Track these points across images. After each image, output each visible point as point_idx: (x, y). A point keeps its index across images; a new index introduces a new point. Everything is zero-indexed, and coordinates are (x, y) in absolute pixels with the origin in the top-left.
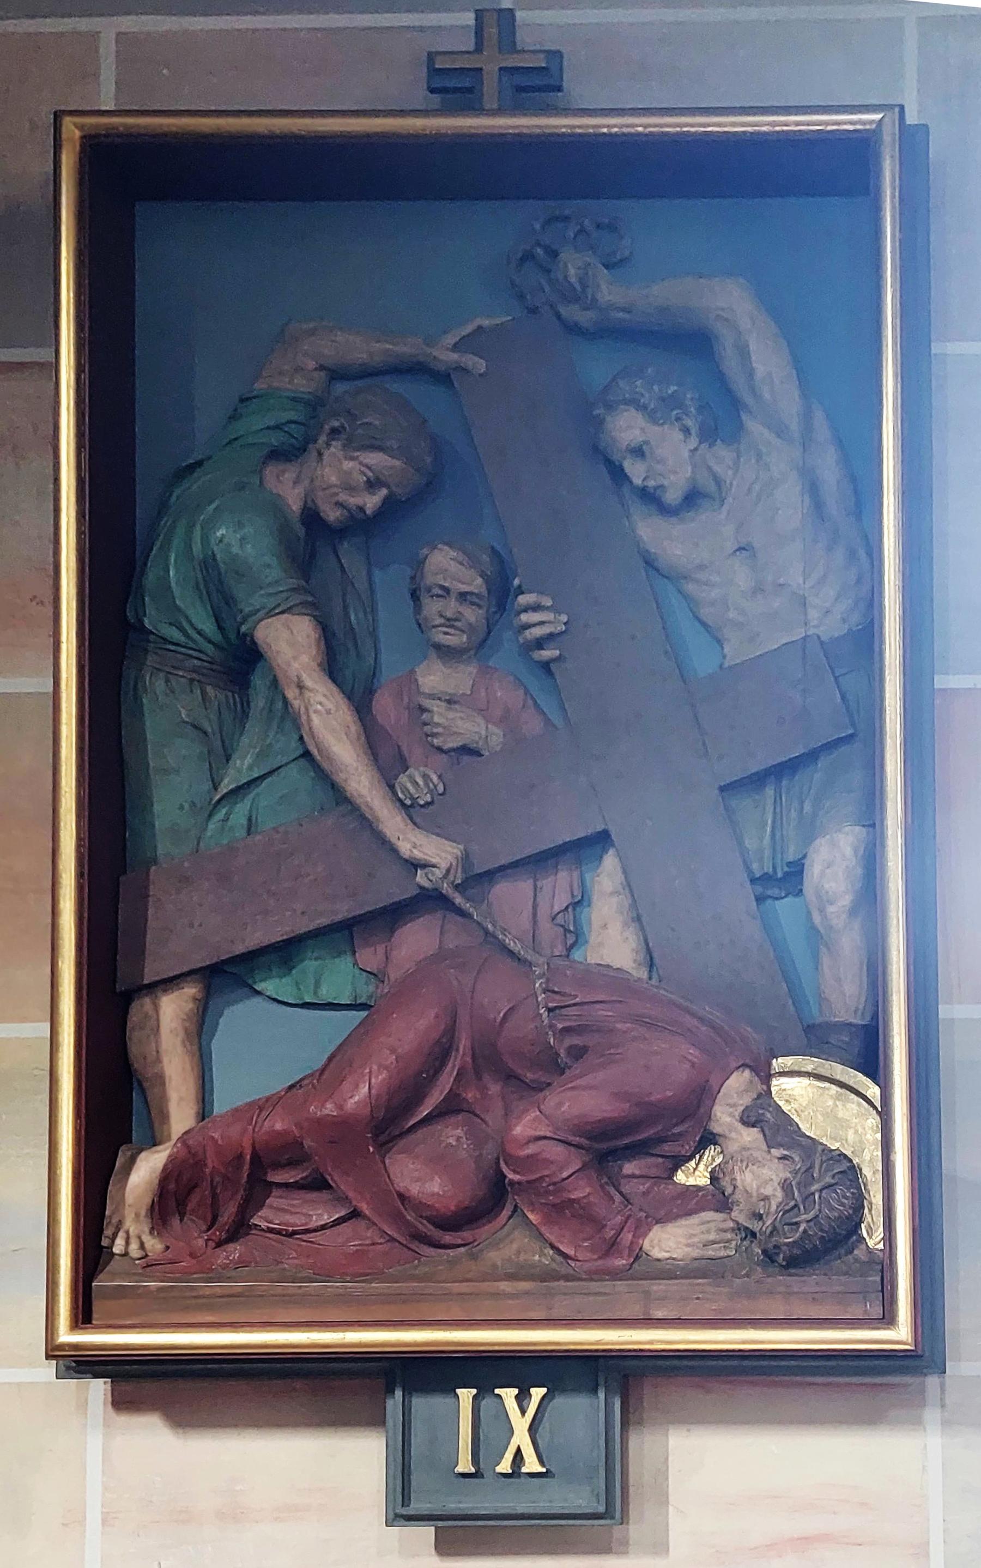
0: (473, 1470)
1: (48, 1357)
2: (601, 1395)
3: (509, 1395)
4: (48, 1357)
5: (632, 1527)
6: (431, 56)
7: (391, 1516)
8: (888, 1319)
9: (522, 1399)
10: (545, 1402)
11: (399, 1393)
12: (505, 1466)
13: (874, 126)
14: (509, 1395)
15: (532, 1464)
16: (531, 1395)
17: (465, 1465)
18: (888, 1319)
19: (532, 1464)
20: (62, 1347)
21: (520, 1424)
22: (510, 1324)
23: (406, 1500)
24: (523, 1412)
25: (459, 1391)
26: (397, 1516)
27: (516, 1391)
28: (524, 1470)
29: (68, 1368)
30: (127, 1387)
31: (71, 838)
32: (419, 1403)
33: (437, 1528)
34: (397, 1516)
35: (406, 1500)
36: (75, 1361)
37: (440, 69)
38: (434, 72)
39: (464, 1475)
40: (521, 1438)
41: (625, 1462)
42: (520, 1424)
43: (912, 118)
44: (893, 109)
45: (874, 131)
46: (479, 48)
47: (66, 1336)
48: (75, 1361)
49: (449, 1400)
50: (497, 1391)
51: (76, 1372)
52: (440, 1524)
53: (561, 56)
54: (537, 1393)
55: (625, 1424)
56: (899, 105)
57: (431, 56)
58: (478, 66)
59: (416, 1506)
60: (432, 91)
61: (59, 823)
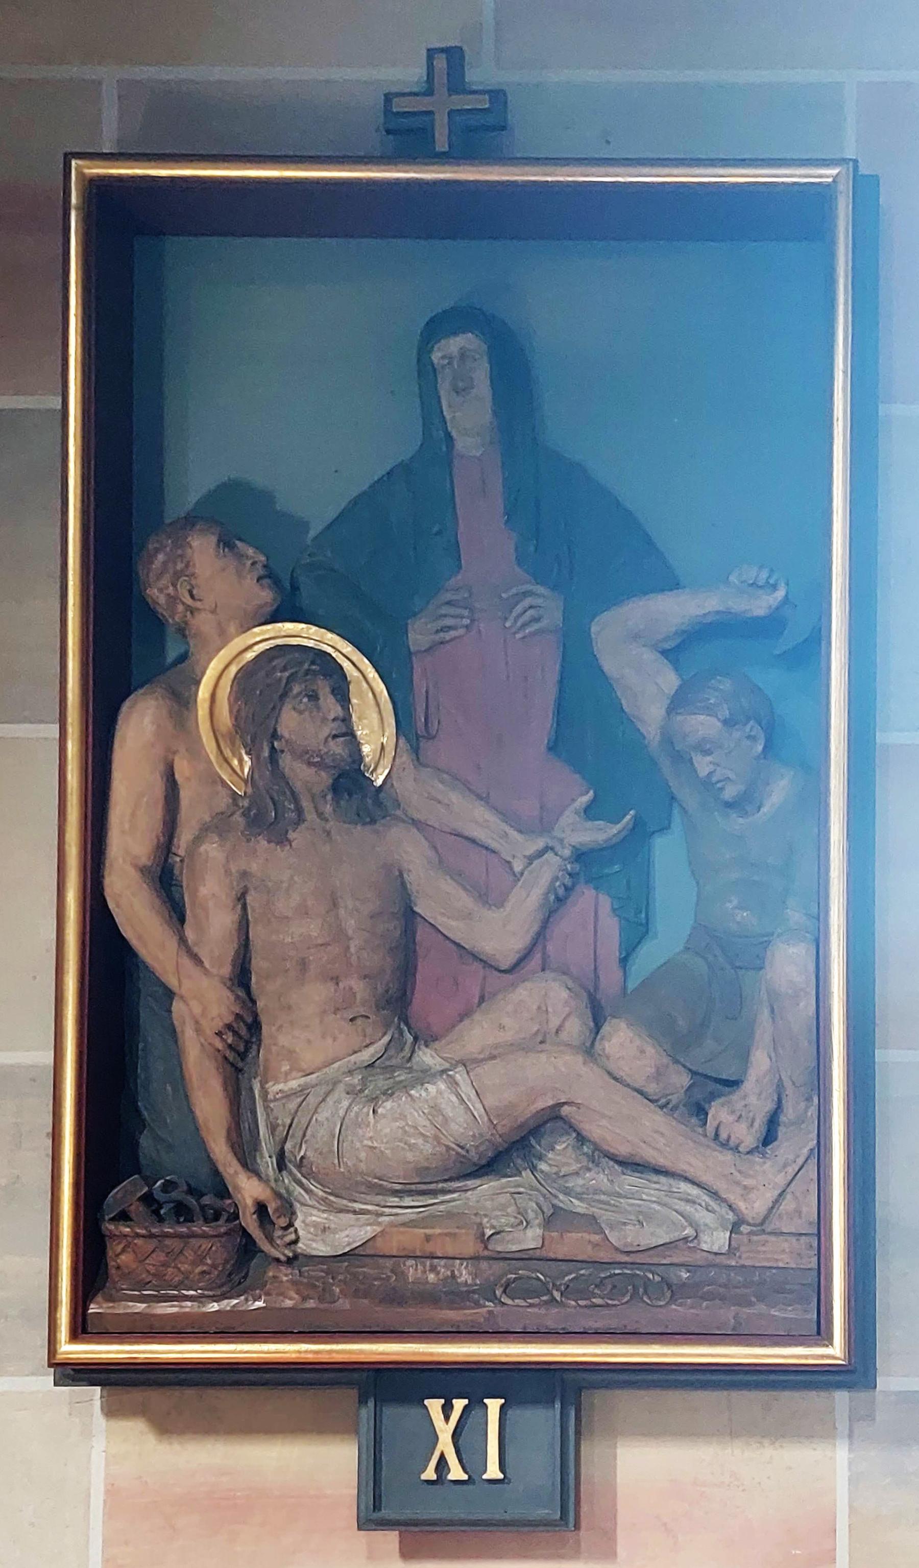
0: (501, 1476)
1: (50, 1365)
2: (558, 1406)
3: (434, 1406)
4: (50, 1365)
6: (388, 98)
9: (447, 1410)
11: (371, 1404)
12: (430, 1474)
13: (830, 180)
15: (456, 1473)
19: (456, 1473)
20: (60, 1357)
21: (445, 1431)
22: (155, 1337)
23: (377, 1507)
25: (426, 1402)
28: (451, 1477)
32: (390, 1412)
36: (73, 1370)
37: (398, 113)
38: (387, 111)
39: (429, 1482)
40: (445, 1444)
41: (377, 1478)
42: (445, 1431)
43: (863, 170)
44: (848, 164)
45: (828, 185)
48: (73, 1370)
49: (414, 1412)
50: (486, 1401)
52: (403, 1528)
53: (505, 94)
54: (459, 1404)
55: (578, 1433)
57: (388, 98)
59: (385, 1513)
60: (388, 132)
61: (80, 853)
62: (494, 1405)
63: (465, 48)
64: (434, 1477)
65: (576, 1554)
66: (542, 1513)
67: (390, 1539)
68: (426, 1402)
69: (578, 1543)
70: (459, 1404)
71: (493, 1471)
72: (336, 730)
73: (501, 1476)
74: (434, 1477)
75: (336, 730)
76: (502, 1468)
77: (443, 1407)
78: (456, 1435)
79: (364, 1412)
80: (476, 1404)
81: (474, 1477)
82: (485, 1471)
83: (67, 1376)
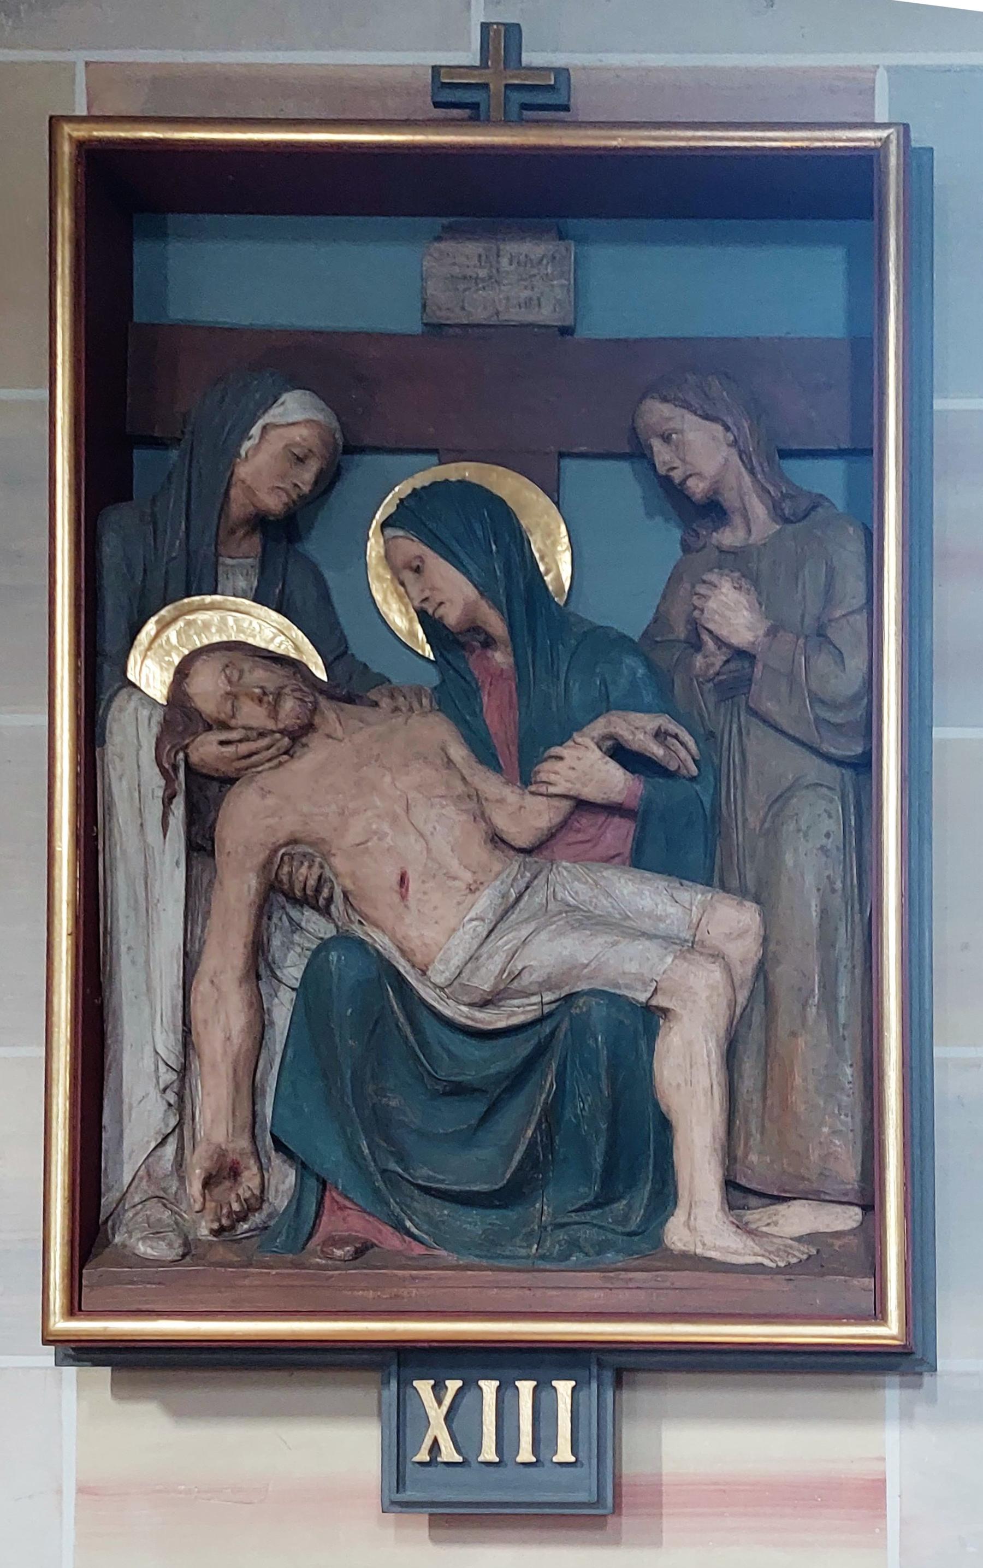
1: (46, 1342)
2: (594, 1386)
3: (424, 1387)
4: (46, 1342)
5: (624, 1520)
7: (387, 1503)
8: (878, 1314)
9: (439, 1390)
10: (575, 1396)
12: (424, 1456)
13: (879, 144)
14: (424, 1387)
15: (449, 1453)
16: (446, 1388)
17: (489, 1453)
18: (878, 1314)
19: (449, 1453)
21: (436, 1414)
23: (400, 1484)
24: (440, 1403)
26: (393, 1503)
27: (497, 1383)
29: (67, 1356)
30: (125, 1374)
31: (179, 836)
33: (431, 1515)
34: (393, 1503)
35: (401, 1486)
39: (421, 1464)
40: (438, 1429)
42: (436, 1414)
45: (875, 149)
46: (484, 65)
47: (61, 1324)
50: (517, 1383)
51: (74, 1360)
52: (435, 1510)
54: (453, 1385)
56: (904, 124)
58: (48, 119)
59: (410, 1495)
60: (437, 105)
62: (564, 1388)
63: (524, 29)
64: (428, 1459)
65: (616, 1541)
66: (582, 1497)
67: (420, 1522)
68: (517, 1383)
69: (618, 1532)
70: (453, 1385)
71: (525, 1455)
72: (507, 647)
73: (573, 1459)
74: (428, 1459)
75: (507, 647)
76: (574, 1452)
77: (433, 1387)
78: (448, 1418)
79: (385, 1393)
80: (470, 1385)
81: (471, 1459)
82: (556, 1453)
83: (67, 1356)
